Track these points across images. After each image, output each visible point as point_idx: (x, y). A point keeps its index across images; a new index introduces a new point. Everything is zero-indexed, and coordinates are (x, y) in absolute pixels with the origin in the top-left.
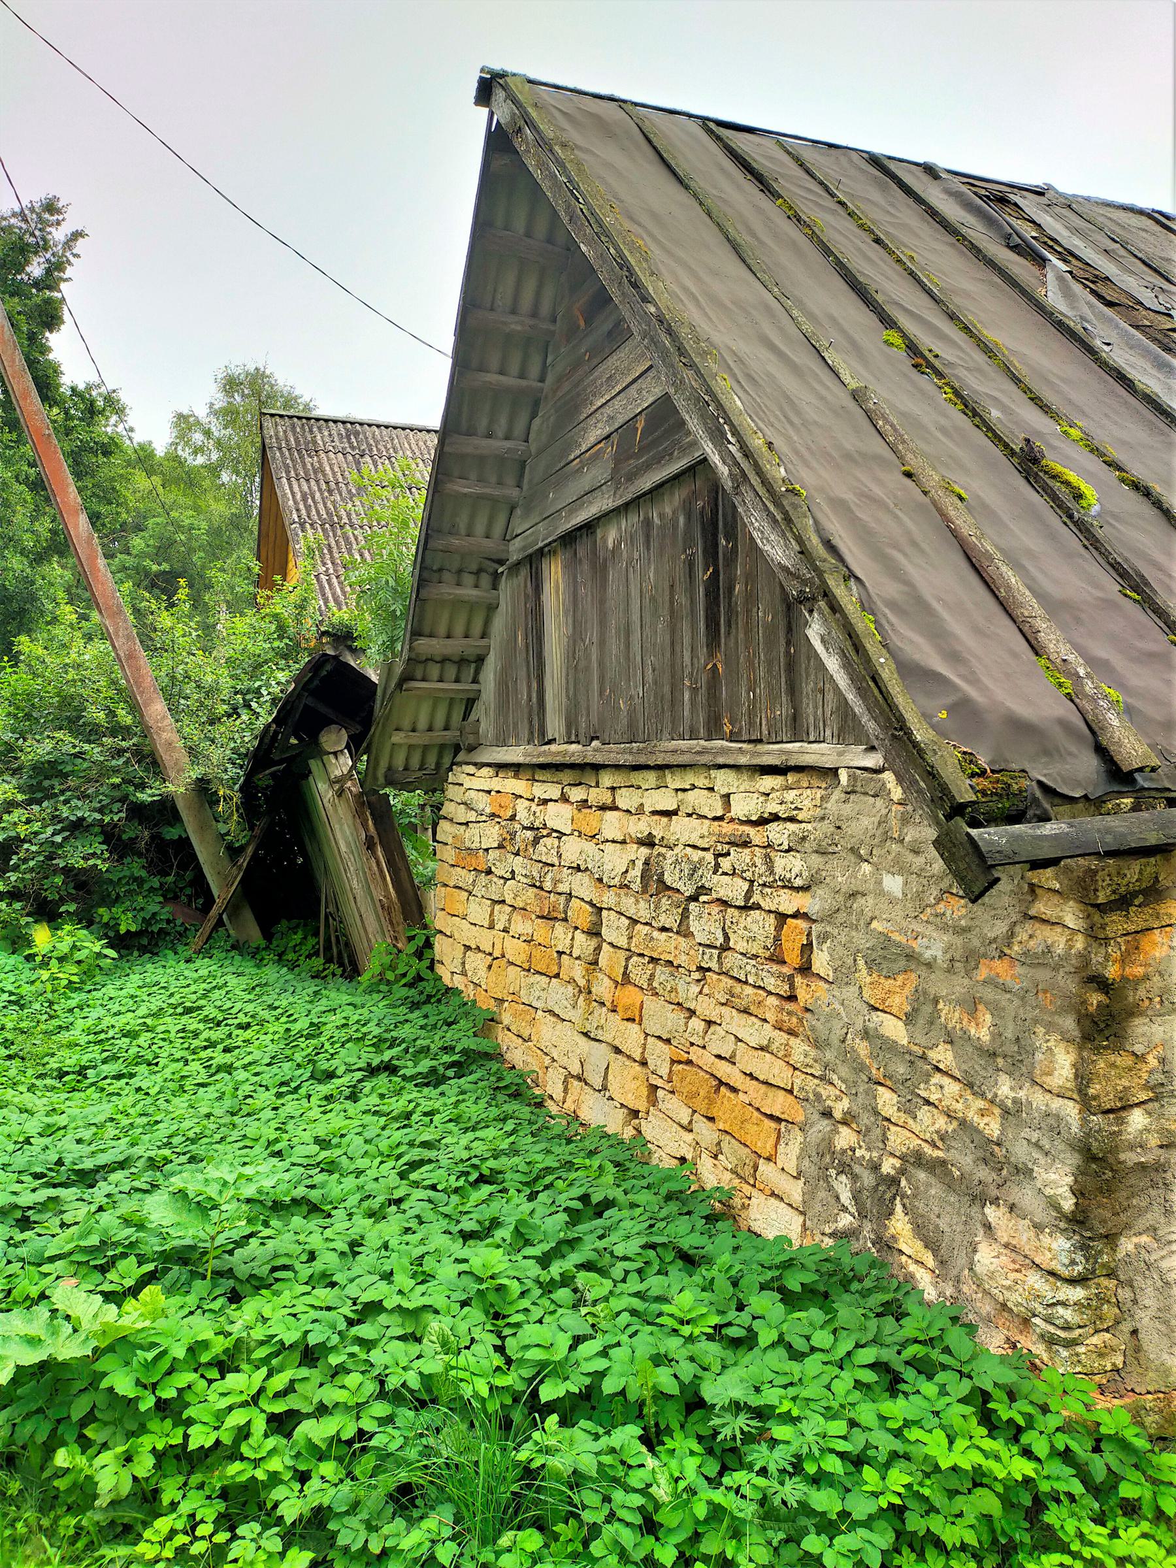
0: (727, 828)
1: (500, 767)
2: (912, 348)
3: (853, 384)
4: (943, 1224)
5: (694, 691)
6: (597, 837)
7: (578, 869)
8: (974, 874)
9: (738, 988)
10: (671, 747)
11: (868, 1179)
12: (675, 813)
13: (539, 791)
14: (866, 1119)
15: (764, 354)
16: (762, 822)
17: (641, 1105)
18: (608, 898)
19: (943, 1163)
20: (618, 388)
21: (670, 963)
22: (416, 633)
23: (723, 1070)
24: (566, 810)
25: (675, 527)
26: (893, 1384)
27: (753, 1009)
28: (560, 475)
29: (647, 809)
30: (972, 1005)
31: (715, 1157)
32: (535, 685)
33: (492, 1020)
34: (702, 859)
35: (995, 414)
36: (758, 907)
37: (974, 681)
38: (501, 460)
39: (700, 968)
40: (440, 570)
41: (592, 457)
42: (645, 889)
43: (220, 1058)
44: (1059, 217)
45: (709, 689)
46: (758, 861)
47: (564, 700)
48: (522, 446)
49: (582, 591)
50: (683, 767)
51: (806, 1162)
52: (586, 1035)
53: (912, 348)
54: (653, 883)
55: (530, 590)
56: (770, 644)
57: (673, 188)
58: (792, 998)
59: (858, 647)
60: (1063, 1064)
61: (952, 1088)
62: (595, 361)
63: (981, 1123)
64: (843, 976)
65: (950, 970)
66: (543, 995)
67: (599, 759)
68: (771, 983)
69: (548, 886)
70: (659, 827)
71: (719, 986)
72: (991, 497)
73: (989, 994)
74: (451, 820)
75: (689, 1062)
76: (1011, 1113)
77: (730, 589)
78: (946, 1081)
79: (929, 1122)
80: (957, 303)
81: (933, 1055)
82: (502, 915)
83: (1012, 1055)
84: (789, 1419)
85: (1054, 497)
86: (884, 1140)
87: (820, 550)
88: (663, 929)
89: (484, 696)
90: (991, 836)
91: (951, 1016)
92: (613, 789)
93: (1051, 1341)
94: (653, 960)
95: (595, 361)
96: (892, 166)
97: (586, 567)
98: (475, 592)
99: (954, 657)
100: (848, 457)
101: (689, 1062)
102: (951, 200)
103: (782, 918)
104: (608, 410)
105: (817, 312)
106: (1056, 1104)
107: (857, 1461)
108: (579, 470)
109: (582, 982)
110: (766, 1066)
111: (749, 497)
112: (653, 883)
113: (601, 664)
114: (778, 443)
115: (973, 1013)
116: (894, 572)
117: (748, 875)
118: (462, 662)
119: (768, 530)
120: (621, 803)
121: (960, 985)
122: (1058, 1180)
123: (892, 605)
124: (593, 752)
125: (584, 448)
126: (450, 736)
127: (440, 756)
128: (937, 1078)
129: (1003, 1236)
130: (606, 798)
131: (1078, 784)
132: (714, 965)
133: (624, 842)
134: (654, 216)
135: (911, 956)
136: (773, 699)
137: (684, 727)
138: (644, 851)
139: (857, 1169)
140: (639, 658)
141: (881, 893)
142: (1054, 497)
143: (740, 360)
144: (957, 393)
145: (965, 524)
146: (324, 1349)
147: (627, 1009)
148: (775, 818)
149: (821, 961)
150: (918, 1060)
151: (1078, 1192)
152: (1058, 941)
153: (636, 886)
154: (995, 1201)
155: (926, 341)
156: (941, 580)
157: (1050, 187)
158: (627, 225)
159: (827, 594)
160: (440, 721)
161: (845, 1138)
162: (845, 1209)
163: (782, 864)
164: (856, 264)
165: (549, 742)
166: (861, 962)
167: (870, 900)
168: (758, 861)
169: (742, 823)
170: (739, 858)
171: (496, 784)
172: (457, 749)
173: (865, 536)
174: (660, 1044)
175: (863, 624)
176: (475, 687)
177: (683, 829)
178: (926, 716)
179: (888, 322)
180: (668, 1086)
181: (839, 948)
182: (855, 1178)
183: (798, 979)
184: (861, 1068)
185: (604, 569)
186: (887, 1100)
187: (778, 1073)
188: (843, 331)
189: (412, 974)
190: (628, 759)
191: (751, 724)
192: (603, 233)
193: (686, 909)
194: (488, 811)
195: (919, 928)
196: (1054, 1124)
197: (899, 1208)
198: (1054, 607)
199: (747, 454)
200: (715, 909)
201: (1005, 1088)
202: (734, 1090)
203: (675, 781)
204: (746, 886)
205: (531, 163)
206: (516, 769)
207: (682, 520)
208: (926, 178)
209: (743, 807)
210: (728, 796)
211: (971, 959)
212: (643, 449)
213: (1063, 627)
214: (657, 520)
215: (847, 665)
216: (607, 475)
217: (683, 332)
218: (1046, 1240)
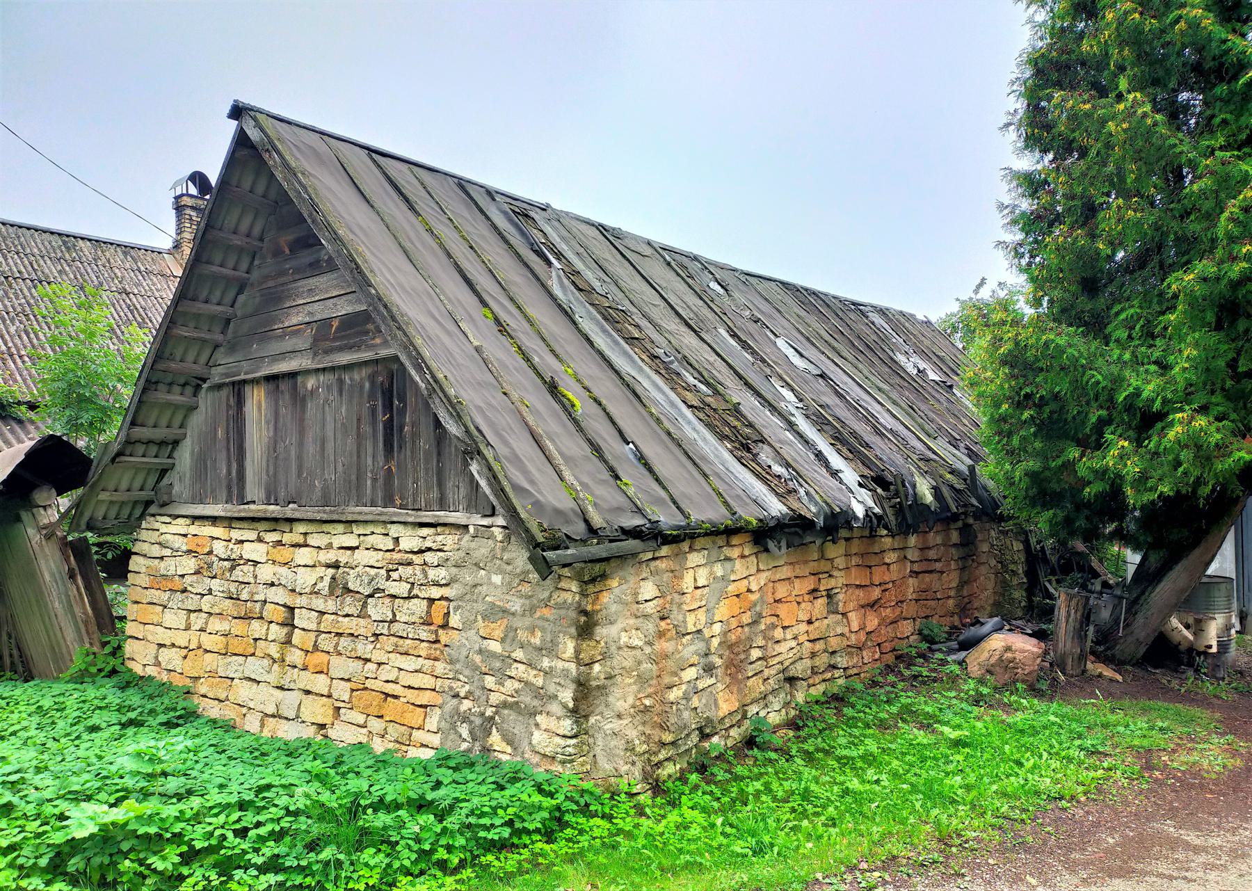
0: (396, 556)
1: (195, 518)
2: (497, 320)
3: (476, 343)
4: (516, 731)
5: (375, 480)
6: (290, 567)
7: (272, 584)
8: (545, 569)
9: (401, 642)
10: (353, 511)
11: (478, 721)
12: (357, 548)
13: (236, 534)
14: (478, 693)
15: (433, 323)
16: (421, 552)
17: (328, 721)
18: (299, 601)
19: (517, 703)
20: (317, 298)
21: (352, 635)
22: (133, 423)
23: (389, 688)
24: (262, 548)
25: (362, 387)
26: (502, 788)
27: (411, 652)
28: (264, 334)
29: (335, 545)
30: (532, 629)
31: (383, 737)
32: (235, 466)
33: (188, 692)
34: (376, 575)
35: (536, 359)
36: (417, 597)
37: (540, 493)
38: (212, 318)
39: (375, 635)
40: (157, 382)
41: (295, 332)
42: (331, 593)
43: (819, 646)
44: (553, 227)
45: (385, 480)
46: (418, 573)
47: (264, 476)
48: (230, 310)
49: (283, 411)
50: (366, 522)
51: (443, 723)
52: (281, 688)
53: (497, 320)
54: (340, 589)
55: (232, 402)
56: (427, 461)
57: (365, 206)
58: (437, 641)
59: (495, 477)
60: (569, 647)
61: (522, 667)
62: (297, 277)
63: (534, 680)
64: (468, 625)
65: (523, 615)
66: (241, 668)
67: (297, 515)
68: (424, 636)
69: (244, 596)
70: (344, 557)
71: (389, 643)
72: (540, 406)
73: (540, 623)
74: (145, 556)
75: (366, 689)
76: (547, 673)
77: (401, 428)
78: (519, 665)
79: (510, 685)
80: (514, 290)
81: (514, 655)
82: (198, 621)
83: (550, 649)
84: (466, 800)
85: (564, 406)
86: (488, 699)
87: (475, 433)
88: (347, 615)
89: (177, 468)
90: (549, 555)
91: (522, 635)
92: (306, 534)
93: (563, 762)
94: (339, 635)
95: (297, 277)
96: (469, 188)
97: (287, 396)
98: (179, 398)
99: (532, 482)
100: (479, 384)
101: (366, 689)
102: (502, 216)
103: (431, 601)
104: (307, 308)
105: (451, 296)
106: (567, 665)
107: (494, 809)
108: (282, 337)
109: (276, 656)
110: (417, 680)
111: (437, 401)
112: (340, 589)
113: (300, 458)
114: (449, 376)
115: (533, 633)
116: (506, 443)
117: (411, 580)
118: (162, 443)
119: (448, 418)
120: (311, 541)
121: (527, 621)
122: (567, 696)
123: (506, 458)
124: (291, 511)
125: (287, 324)
126: (146, 494)
127: (133, 508)
128: (516, 665)
129: (543, 726)
130: (301, 540)
131: (578, 534)
132: (385, 632)
133: (314, 566)
134: (361, 228)
135: (505, 611)
136: (429, 489)
137: (367, 499)
138: (331, 571)
139: (472, 718)
140: (332, 458)
141: (490, 583)
142: (564, 406)
143: (423, 327)
144: (520, 348)
145: (530, 420)
146: (251, 802)
147: (316, 666)
148: (429, 549)
149: (455, 620)
150: (508, 660)
151: (575, 700)
152: (568, 597)
153: (326, 591)
154: (541, 713)
155: (503, 316)
156: (524, 447)
157: (548, 206)
158: (352, 236)
159: (479, 453)
160: (137, 485)
161: (466, 704)
162: (464, 740)
163: (432, 574)
164: (465, 265)
165: (248, 503)
166: (479, 617)
167: (485, 587)
168: (418, 573)
169: (407, 552)
170: (405, 571)
171: (194, 529)
172: (148, 503)
173: (491, 424)
174: (343, 683)
175: (496, 467)
176: (170, 461)
177: (362, 557)
178: (524, 507)
179: (484, 304)
180: (349, 706)
181: (467, 614)
182: (471, 722)
183: (440, 631)
184: (477, 668)
185: (304, 400)
186: (490, 681)
187: (428, 681)
188: (465, 309)
189: (109, 668)
190: (325, 517)
191: (414, 501)
192: (336, 238)
193: (365, 602)
194: (184, 548)
195: (508, 597)
196: (566, 673)
197: (494, 730)
198: (568, 459)
199: (436, 381)
200: (387, 600)
201: (546, 663)
202: (396, 697)
203: (358, 530)
204: (409, 586)
205: (279, 176)
206: (214, 520)
207: (367, 385)
208: (488, 199)
209: (405, 544)
210: (397, 539)
211: (533, 609)
212: (335, 339)
213: (571, 469)
214: (348, 381)
215: (490, 484)
216: (307, 345)
217: (394, 309)
218: (562, 722)
